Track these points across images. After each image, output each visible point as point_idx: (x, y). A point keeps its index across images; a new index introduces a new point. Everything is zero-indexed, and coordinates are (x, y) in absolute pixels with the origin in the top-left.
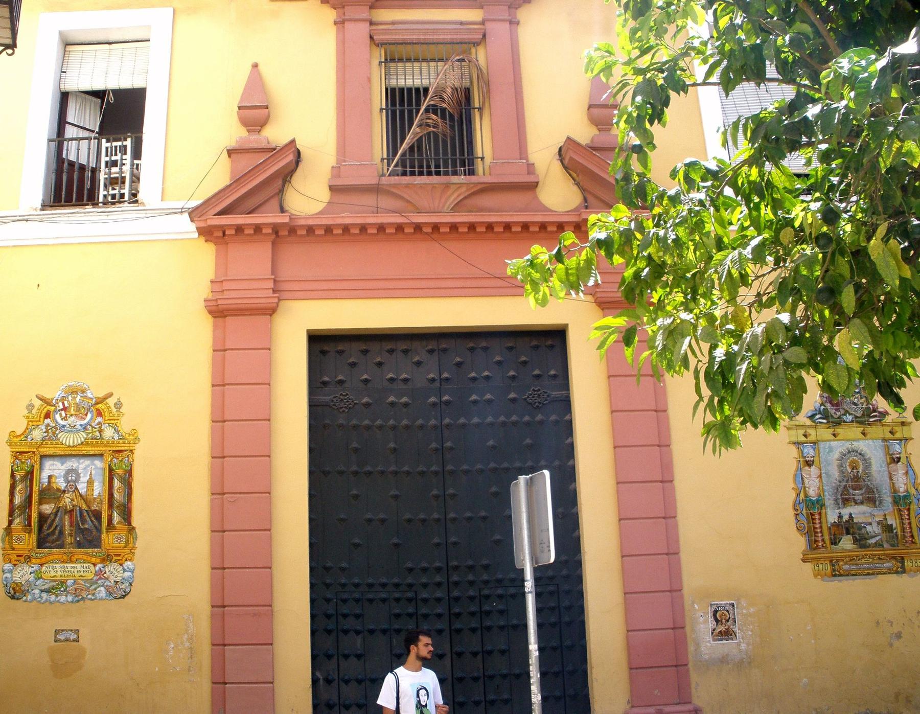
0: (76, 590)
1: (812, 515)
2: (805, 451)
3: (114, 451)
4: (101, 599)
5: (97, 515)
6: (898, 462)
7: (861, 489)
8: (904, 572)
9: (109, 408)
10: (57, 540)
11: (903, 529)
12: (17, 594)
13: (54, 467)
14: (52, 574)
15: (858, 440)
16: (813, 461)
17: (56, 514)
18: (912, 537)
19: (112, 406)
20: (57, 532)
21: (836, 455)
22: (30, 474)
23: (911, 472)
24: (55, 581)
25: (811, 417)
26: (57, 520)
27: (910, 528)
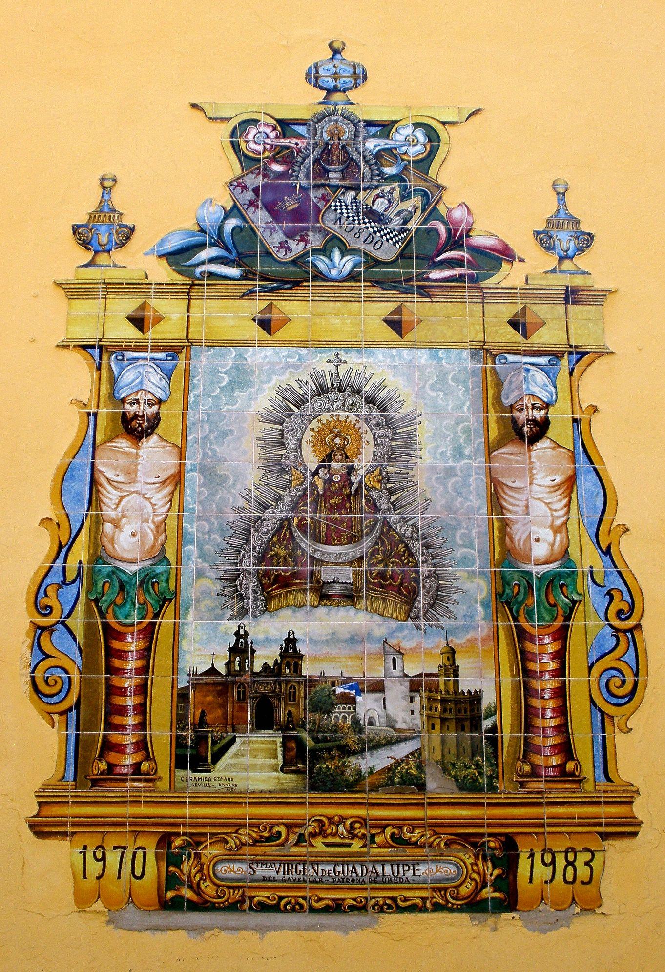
1: (110, 633)
2: (129, 376)
6: (534, 439)
7: (352, 539)
8: (509, 902)
11: (528, 718)
16: (155, 421)
18: (566, 749)
21: (264, 398)
23: (587, 483)
25: (178, 257)
27: (562, 711)
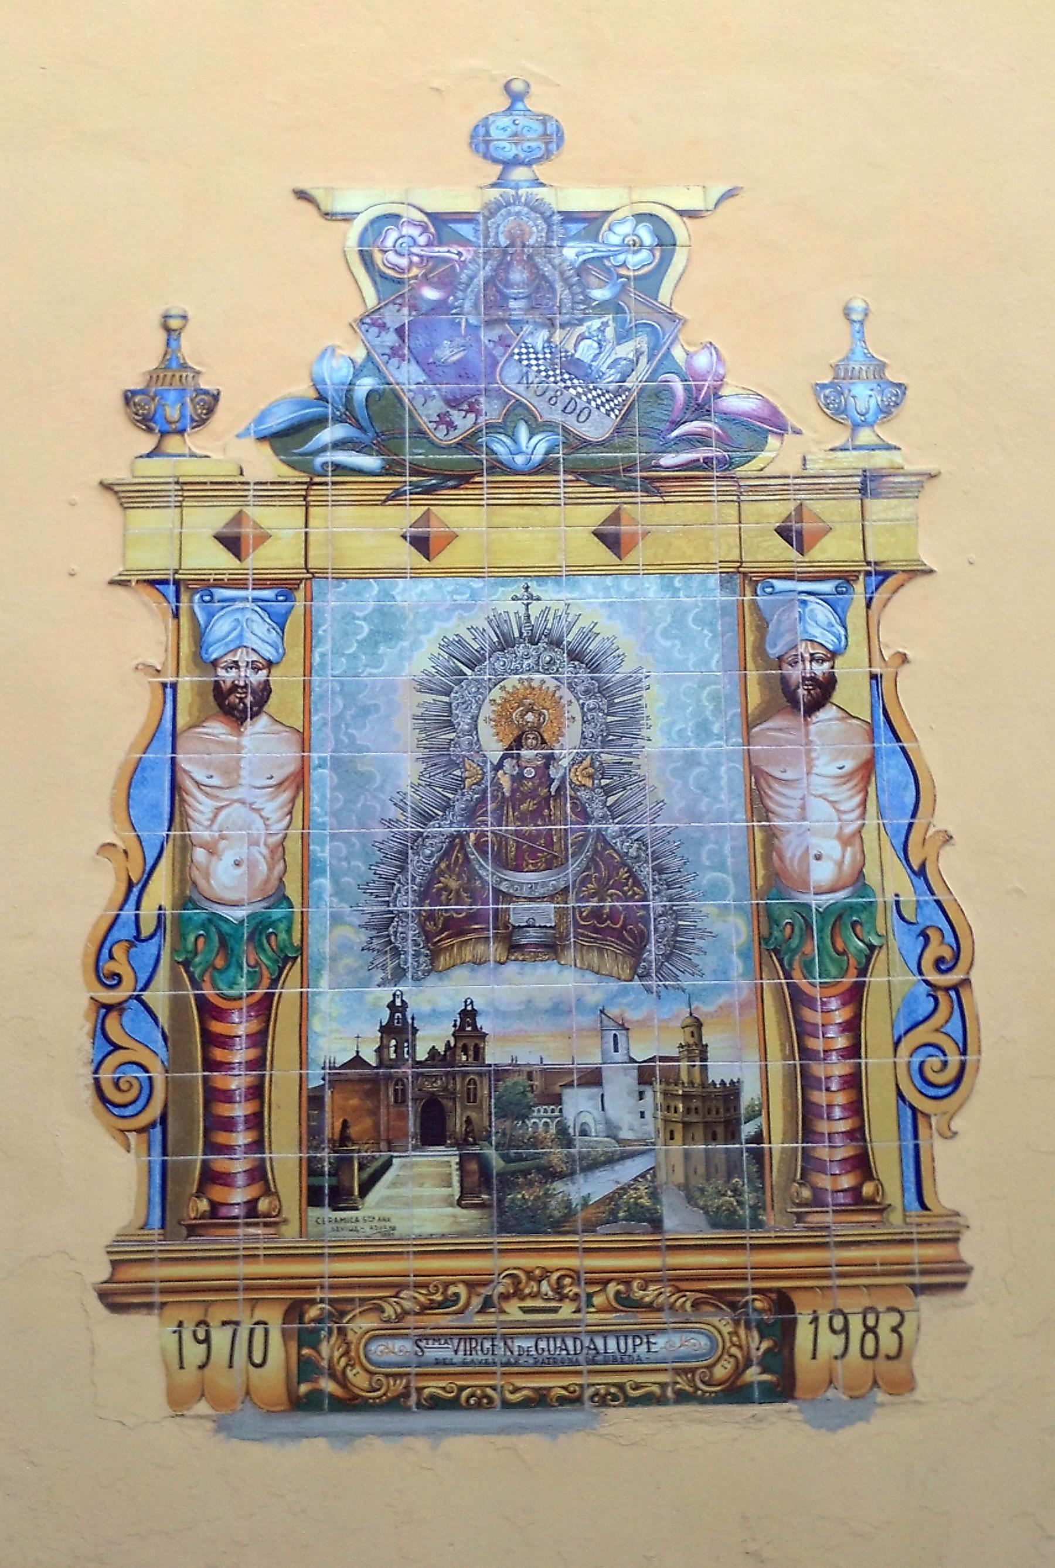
1: (208, 1010)
2: (222, 627)
6: (815, 706)
7: (552, 863)
8: (783, 1387)
11: (807, 1120)
15: (576, 573)
16: (264, 693)
18: (862, 1164)
21: (422, 657)
23: (891, 769)
25: (288, 438)
27: (856, 1109)
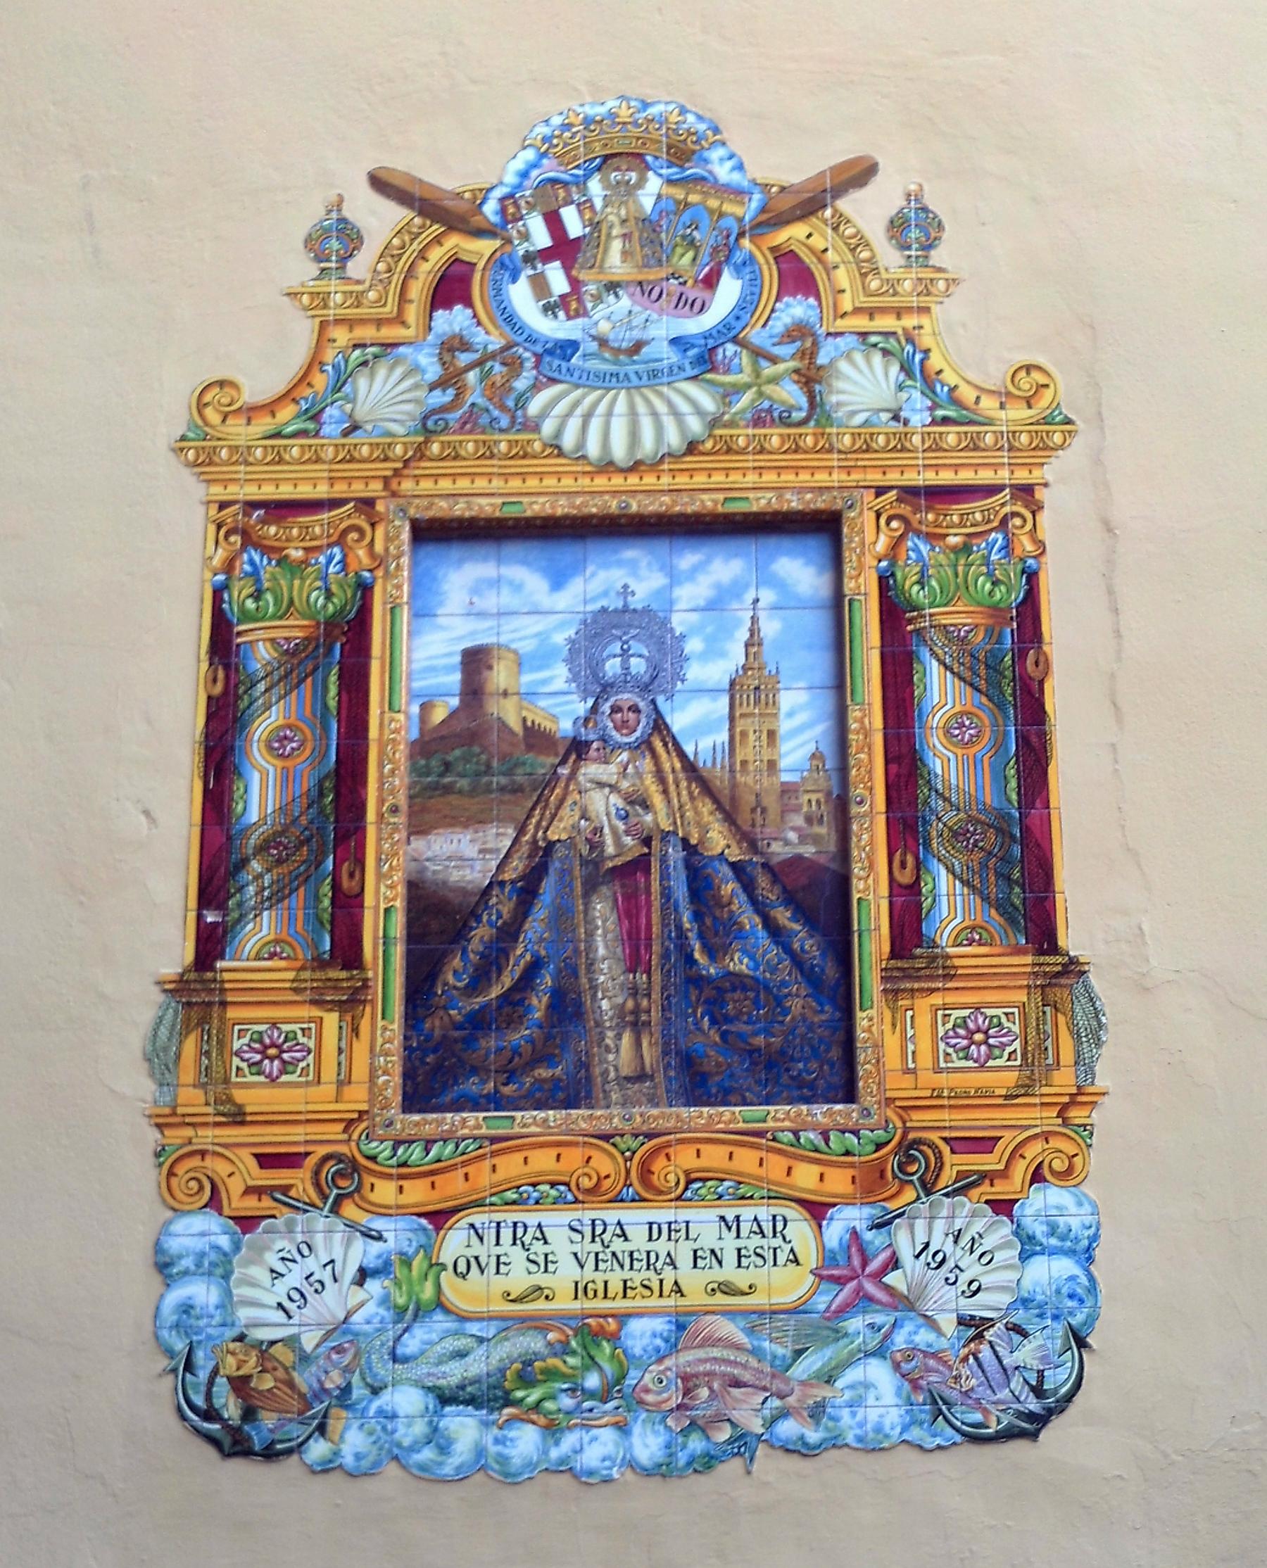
0: (688, 1382)
3: (910, 493)
4: (873, 1446)
5: (822, 897)
9: (859, 242)
10: (541, 1057)
12: (268, 1420)
13: (506, 599)
14: (519, 1277)
17: (528, 891)
19: (876, 233)
20: (539, 1004)
22: (346, 644)
24: (538, 1324)
26: (536, 926)
